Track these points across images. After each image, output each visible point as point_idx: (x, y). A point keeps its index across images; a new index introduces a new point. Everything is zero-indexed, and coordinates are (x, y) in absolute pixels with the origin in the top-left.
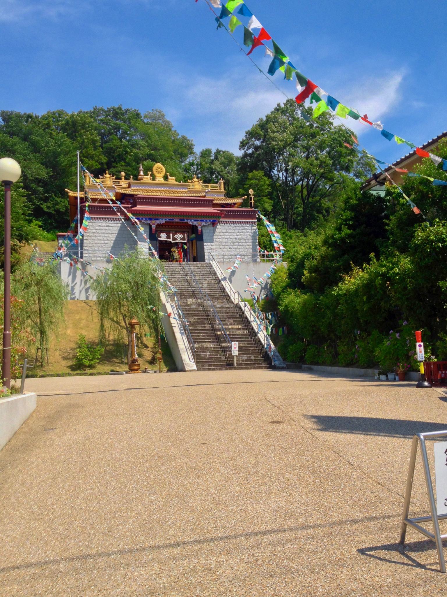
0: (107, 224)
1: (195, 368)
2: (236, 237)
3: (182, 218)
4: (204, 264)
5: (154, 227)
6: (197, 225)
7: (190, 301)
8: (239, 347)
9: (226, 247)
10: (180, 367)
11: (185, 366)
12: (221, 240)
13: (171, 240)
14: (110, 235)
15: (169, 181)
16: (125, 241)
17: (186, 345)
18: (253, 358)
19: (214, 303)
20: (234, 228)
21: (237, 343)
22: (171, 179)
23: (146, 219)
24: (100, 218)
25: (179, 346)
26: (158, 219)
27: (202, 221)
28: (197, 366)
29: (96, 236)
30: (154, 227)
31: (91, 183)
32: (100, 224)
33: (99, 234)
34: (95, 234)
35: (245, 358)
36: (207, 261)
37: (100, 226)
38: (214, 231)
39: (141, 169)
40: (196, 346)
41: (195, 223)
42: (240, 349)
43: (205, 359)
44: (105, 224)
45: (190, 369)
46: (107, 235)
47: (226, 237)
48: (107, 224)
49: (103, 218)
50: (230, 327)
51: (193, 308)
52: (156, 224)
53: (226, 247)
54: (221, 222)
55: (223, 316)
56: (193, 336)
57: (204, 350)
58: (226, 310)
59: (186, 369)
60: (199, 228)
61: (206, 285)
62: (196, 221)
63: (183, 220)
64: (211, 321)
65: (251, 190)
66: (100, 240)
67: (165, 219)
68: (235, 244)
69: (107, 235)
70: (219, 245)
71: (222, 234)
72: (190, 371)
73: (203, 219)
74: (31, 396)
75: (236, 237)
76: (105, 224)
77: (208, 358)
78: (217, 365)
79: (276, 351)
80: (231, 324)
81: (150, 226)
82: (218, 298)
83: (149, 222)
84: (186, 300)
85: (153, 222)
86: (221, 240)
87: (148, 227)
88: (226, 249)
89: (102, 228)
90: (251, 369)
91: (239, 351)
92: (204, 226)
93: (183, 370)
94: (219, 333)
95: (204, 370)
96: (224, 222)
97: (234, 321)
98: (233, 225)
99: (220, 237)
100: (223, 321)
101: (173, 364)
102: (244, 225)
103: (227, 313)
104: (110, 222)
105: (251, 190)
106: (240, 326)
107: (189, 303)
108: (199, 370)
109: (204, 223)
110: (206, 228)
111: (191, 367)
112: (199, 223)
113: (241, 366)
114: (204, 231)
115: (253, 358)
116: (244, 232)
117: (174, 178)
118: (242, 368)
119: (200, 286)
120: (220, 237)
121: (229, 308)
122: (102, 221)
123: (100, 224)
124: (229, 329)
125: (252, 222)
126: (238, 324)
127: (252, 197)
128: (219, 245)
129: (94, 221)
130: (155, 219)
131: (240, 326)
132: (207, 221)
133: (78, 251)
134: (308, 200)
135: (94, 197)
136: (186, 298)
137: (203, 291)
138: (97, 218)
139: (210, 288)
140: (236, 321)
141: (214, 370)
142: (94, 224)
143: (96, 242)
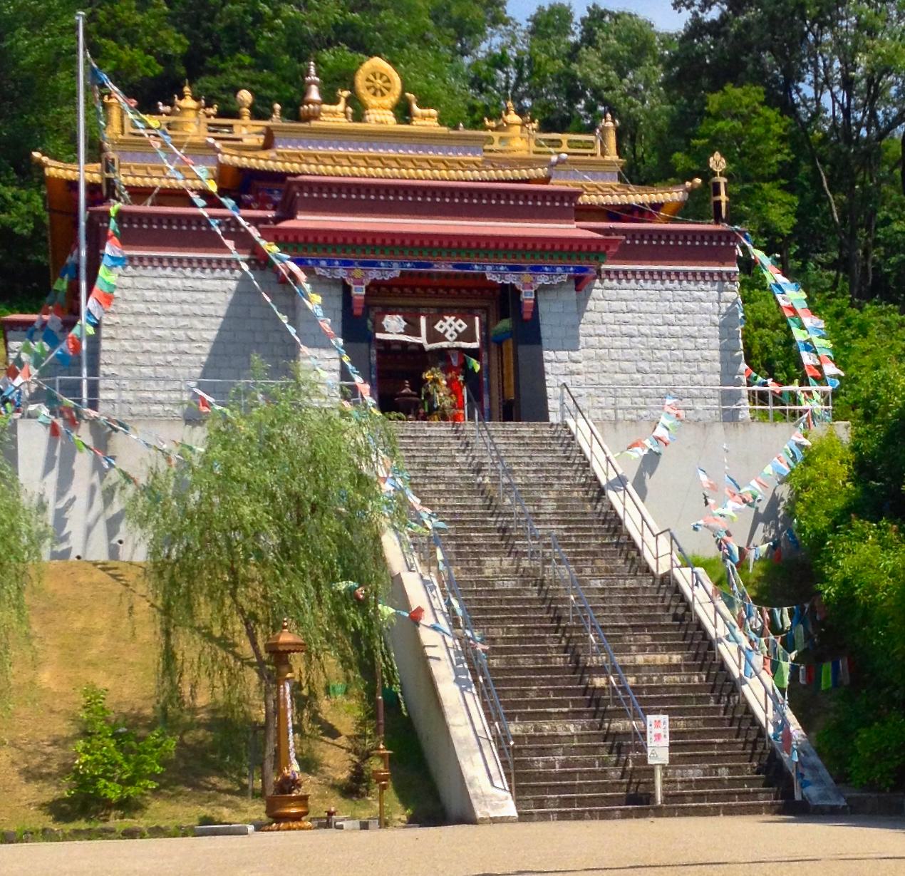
0: (188, 283)
1: (510, 809)
2: (664, 329)
3: (464, 260)
4: (544, 430)
5: (359, 292)
6: (519, 285)
8: (673, 734)
9: (626, 365)
10: (454, 807)
11: (474, 802)
12: (605, 341)
15: (417, 121)
18: (724, 773)
20: (656, 295)
22: (424, 117)
23: (330, 262)
24: (160, 260)
25: (453, 730)
26: (373, 264)
27: (537, 269)
29: (145, 327)
30: (359, 292)
31: (128, 129)
32: (162, 282)
34: (142, 319)
35: (695, 773)
37: (161, 289)
38: (581, 309)
39: (313, 77)
41: (510, 279)
42: (678, 741)
43: (546, 776)
44: (178, 283)
45: (492, 815)
46: (185, 322)
47: (625, 329)
48: (188, 283)
49: (170, 260)
50: (640, 659)
52: (367, 282)
53: (626, 365)
54: (608, 272)
57: (543, 745)
58: (624, 599)
59: (479, 815)
60: (527, 297)
61: (550, 506)
62: (512, 269)
63: (468, 267)
65: (717, 156)
67: (402, 265)
69: (185, 322)
71: (609, 317)
72: (494, 820)
73: (538, 261)
75: (664, 329)
76: (178, 283)
80: (642, 649)
81: (347, 290)
82: (594, 553)
83: (341, 273)
86: (605, 341)
87: (338, 291)
88: (624, 372)
89: (168, 295)
92: (544, 288)
93: (467, 818)
94: (599, 682)
95: (545, 817)
96: (616, 272)
97: (654, 638)
99: (602, 329)
100: (615, 638)
101: (431, 797)
103: (630, 609)
105: (717, 156)
106: (676, 658)
107: (488, 572)
108: (524, 817)
109: (543, 280)
110: (551, 295)
111: (495, 807)
112: (527, 276)
113: (681, 803)
114: (542, 307)
115: (724, 773)
116: (692, 312)
117: (433, 112)
118: (685, 812)
119: (531, 509)
121: (634, 590)
122: (168, 271)
123: (162, 282)
124: (637, 669)
125: (720, 274)
126: (669, 648)
127: (723, 180)
128: (600, 358)
129: (140, 270)
130: (362, 264)
131: (676, 658)
132: (553, 269)
133: (80, 382)
135: (139, 182)
136: (476, 554)
137: (540, 529)
138: (151, 259)
139: (566, 516)
140: (664, 637)
141: (579, 816)
142: (138, 283)
143: (147, 346)
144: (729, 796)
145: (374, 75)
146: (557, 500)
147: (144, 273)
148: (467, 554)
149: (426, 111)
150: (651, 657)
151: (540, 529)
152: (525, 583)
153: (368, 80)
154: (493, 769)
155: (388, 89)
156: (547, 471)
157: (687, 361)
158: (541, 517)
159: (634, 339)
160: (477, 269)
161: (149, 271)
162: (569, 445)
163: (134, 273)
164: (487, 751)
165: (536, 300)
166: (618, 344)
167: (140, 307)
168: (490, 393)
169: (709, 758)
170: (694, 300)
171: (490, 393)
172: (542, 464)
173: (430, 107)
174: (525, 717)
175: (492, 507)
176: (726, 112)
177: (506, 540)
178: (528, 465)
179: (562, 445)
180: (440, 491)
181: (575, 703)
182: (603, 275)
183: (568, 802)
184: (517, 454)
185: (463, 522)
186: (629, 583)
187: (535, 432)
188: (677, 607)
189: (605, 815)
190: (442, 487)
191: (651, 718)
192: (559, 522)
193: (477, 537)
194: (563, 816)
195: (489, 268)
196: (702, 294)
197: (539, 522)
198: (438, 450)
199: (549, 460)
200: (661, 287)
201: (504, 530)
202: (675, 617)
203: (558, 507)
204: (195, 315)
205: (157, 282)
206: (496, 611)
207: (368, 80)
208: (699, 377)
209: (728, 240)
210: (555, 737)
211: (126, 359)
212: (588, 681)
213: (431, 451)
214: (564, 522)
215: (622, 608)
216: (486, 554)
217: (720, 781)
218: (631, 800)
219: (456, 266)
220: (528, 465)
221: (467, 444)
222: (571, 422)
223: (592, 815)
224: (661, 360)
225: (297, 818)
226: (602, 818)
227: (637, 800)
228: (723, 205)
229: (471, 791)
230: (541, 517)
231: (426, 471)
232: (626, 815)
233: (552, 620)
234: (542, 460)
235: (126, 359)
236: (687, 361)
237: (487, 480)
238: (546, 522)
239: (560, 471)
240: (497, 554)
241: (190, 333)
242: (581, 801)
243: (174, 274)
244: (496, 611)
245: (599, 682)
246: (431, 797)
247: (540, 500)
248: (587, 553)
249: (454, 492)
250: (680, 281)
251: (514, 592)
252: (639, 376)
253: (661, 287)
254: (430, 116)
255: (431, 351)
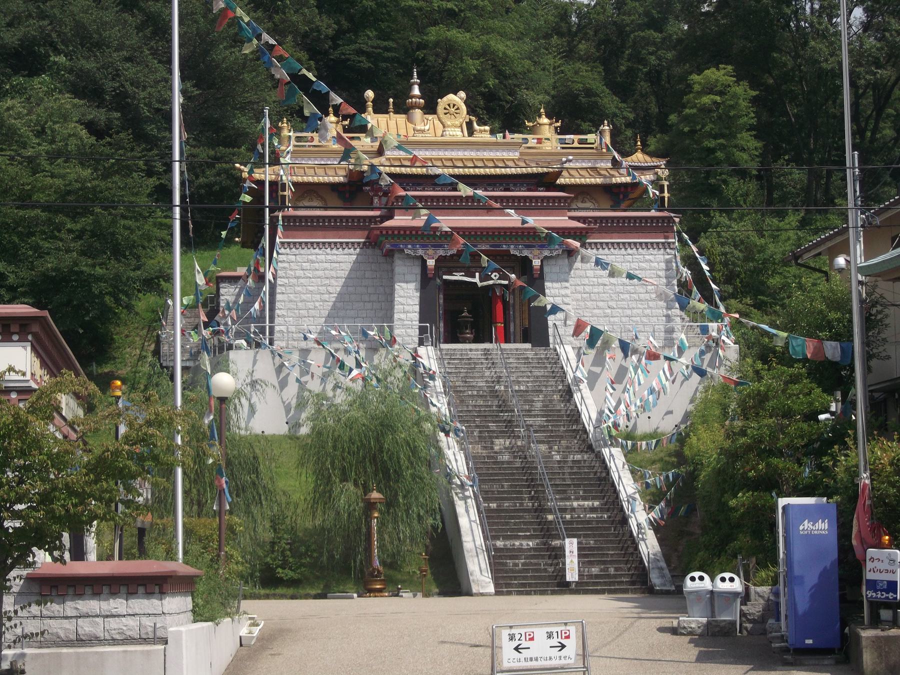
0: (329, 257)
1: (491, 589)
4: (541, 352)
5: (431, 263)
6: (530, 256)
7: (499, 444)
8: (579, 549)
9: (601, 304)
10: (464, 588)
11: (472, 584)
12: (587, 289)
13: (476, 280)
14: (333, 281)
15: (476, 135)
16: (366, 300)
17: (478, 543)
18: (612, 571)
19: (551, 448)
21: (575, 541)
22: (481, 131)
25: (465, 544)
26: (441, 246)
28: (495, 587)
29: (303, 285)
30: (431, 263)
32: (313, 258)
33: (310, 275)
34: (302, 281)
35: (595, 570)
36: (551, 346)
37: (313, 262)
38: (571, 268)
39: (415, 79)
40: (500, 544)
41: (526, 253)
42: (583, 552)
43: (513, 571)
44: (322, 257)
45: (481, 591)
46: (327, 282)
48: (329, 257)
51: (503, 463)
53: (601, 304)
54: (590, 244)
55: (564, 480)
56: (493, 523)
57: (514, 553)
58: (572, 468)
59: (474, 591)
60: (536, 263)
61: (539, 405)
62: (528, 247)
63: (499, 246)
64: (536, 492)
66: (311, 292)
68: (622, 296)
69: (327, 282)
70: (584, 300)
72: (482, 594)
74: (203, 628)
76: (322, 257)
77: (520, 571)
78: (536, 585)
79: (660, 555)
81: (424, 262)
82: (562, 437)
84: (492, 443)
85: (431, 251)
86: (587, 289)
87: (418, 262)
88: (598, 308)
90: (604, 593)
91: (579, 556)
92: (546, 257)
93: (469, 593)
94: (550, 517)
95: (509, 593)
97: (585, 491)
98: (616, 251)
99: (586, 281)
100: (562, 491)
101: (449, 579)
102: (644, 251)
103: (575, 473)
104: (334, 251)
106: (596, 503)
107: (496, 448)
108: (498, 593)
109: (546, 253)
110: (553, 262)
111: (482, 587)
112: (536, 252)
113: (582, 588)
115: (612, 571)
117: (487, 128)
118: (586, 592)
119: (527, 407)
120: (586, 281)
121: (579, 462)
122: (317, 250)
123: (313, 258)
124: (573, 510)
126: (594, 498)
128: (584, 300)
130: (432, 246)
131: (596, 503)
133: (265, 327)
134: (875, 130)
135: (300, 179)
136: (491, 437)
137: (530, 421)
139: (548, 412)
140: (590, 491)
141: (528, 593)
142: (299, 258)
143: (304, 297)
144: (613, 583)
145: (449, 105)
146: (542, 401)
147: (302, 252)
148: (485, 438)
149: (482, 128)
150: (581, 503)
151: (530, 421)
152: (515, 457)
153: (445, 109)
154: (483, 566)
155: (458, 109)
156: (540, 381)
157: (641, 300)
158: (533, 413)
159: (606, 287)
160: (505, 247)
161: (306, 251)
162: (555, 363)
163: (297, 252)
164: (481, 557)
165: (542, 266)
166: (596, 290)
167: (299, 273)
168: (514, 322)
169: (604, 562)
170: (646, 261)
171: (514, 322)
172: (537, 377)
173: (485, 125)
174: (506, 538)
175: (504, 406)
176: (710, 89)
177: (509, 429)
178: (528, 377)
179: (550, 363)
180: (473, 396)
181: (535, 530)
182: (587, 246)
183: (524, 585)
184: (523, 369)
185: (486, 416)
186: (578, 457)
187: (536, 354)
188: (601, 472)
189: (543, 593)
190: (475, 393)
191: (567, 541)
192: (543, 416)
193: (493, 426)
194: (520, 593)
195: (512, 246)
196: (651, 257)
197: (530, 416)
198: (475, 368)
199: (542, 374)
200: (625, 253)
201: (510, 421)
202: (600, 479)
203: (544, 406)
204: (333, 277)
205: (310, 257)
206: (496, 475)
207: (445, 109)
208: (648, 311)
209: (669, 222)
210: (520, 550)
211: (292, 306)
212: (554, 517)
213: (471, 369)
214: (547, 416)
215: (570, 474)
216: (497, 438)
217: (609, 576)
218: (559, 585)
219: (491, 246)
220: (528, 377)
221: (493, 363)
222: (557, 347)
223: (536, 593)
224: (623, 300)
225: (380, 591)
226: (541, 594)
227: (562, 586)
228: (666, 199)
229: (471, 578)
230: (533, 413)
231: (466, 382)
232: (554, 593)
233: (527, 480)
234: (539, 374)
235: (292, 306)
236: (641, 300)
237: (503, 388)
238: (535, 416)
239: (548, 381)
240: (503, 437)
241: (329, 288)
242: (530, 585)
243: (321, 252)
244: (496, 475)
245: (550, 517)
246: (449, 579)
247: (533, 401)
248: (557, 436)
249: (482, 396)
250: (637, 249)
251: (508, 463)
252: (609, 311)
253: (625, 253)
254: (485, 131)
255: (482, 287)
